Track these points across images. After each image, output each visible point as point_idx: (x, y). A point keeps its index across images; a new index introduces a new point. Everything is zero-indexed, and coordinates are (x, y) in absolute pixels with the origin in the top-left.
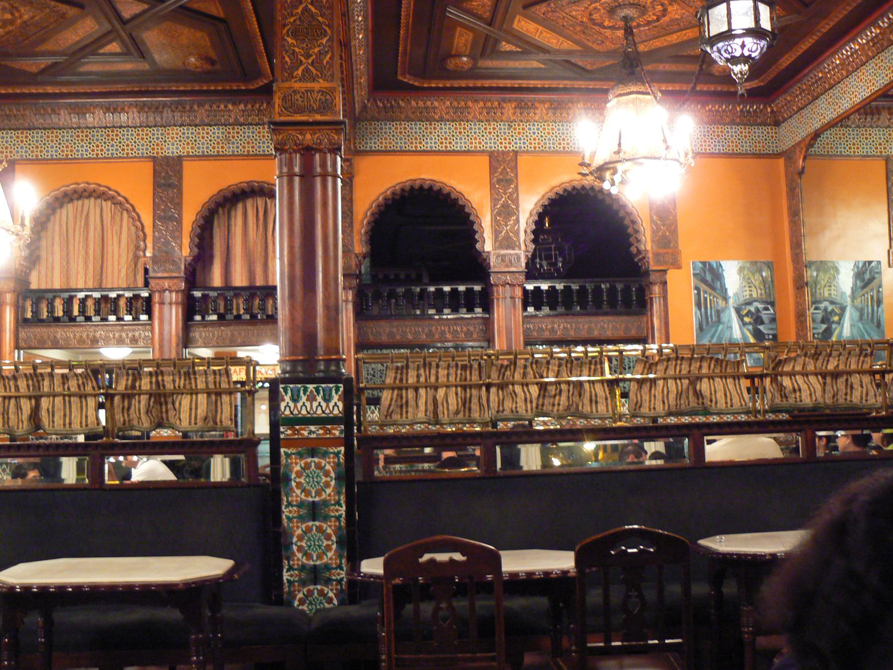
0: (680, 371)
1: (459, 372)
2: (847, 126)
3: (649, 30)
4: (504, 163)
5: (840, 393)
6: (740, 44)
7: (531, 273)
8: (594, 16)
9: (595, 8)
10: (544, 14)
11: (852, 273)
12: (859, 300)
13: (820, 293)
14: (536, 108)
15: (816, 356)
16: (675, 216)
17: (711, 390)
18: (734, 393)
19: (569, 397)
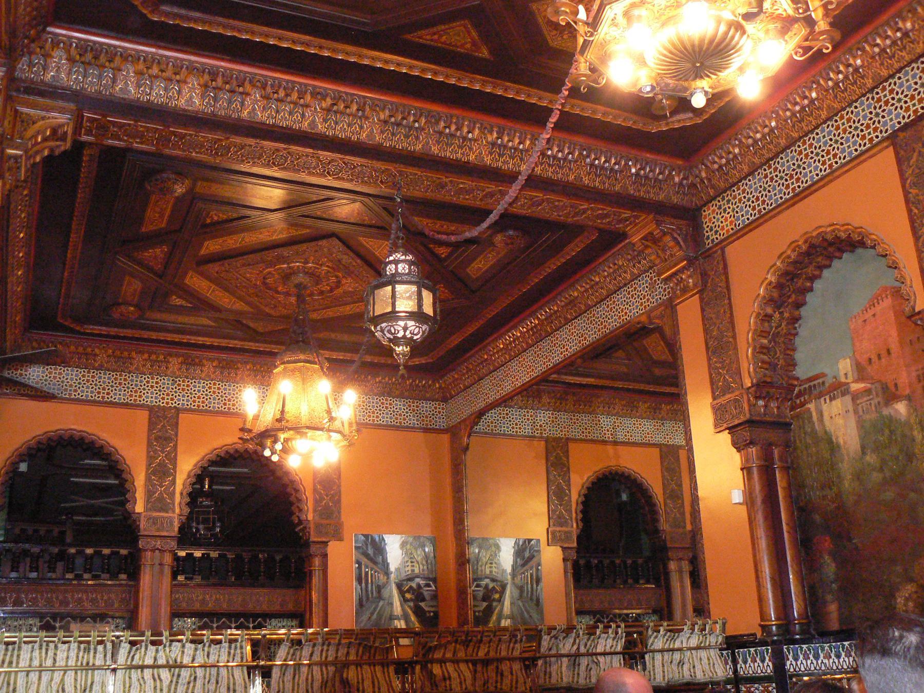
0: (326, 657)
1: (81, 654)
2: (511, 407)
3: (322, 299)
4: (164, 419)
5: (490, 681)
6: (403, 325)
7: (185, 537)
8: (268, 281)
9: (269, 273)
10: (217, 273)
11: (513, 551)
12: (519, 577)
13: (482, 570)
14: (203, 365)
15: (467, 643)
16: (339, 486)
17: (358, 678)
18: (382, 682)
19: (204, 684)
